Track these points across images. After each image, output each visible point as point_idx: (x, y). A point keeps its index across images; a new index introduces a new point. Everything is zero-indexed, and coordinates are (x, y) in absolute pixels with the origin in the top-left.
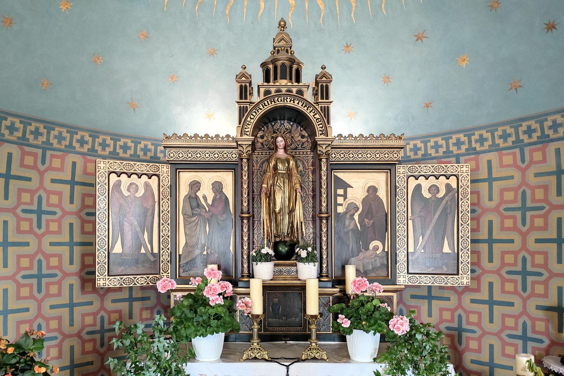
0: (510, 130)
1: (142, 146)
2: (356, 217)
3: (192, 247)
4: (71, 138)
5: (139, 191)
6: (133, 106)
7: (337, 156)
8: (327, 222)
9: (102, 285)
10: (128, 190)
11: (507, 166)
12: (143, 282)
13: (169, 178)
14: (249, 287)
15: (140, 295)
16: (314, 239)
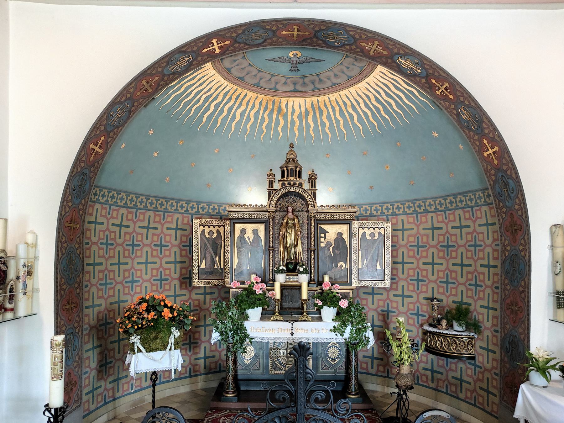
0: (411, 205)
1: (212, 207)
2: (331, 249)
4: (177, 205)
6: (208, 186)
7: (320, 217)
8: (314, 253)
10: (209, 235)
11: (411, 223)
14: (274, 286)
15: (209, 291)
16: (308, 260)
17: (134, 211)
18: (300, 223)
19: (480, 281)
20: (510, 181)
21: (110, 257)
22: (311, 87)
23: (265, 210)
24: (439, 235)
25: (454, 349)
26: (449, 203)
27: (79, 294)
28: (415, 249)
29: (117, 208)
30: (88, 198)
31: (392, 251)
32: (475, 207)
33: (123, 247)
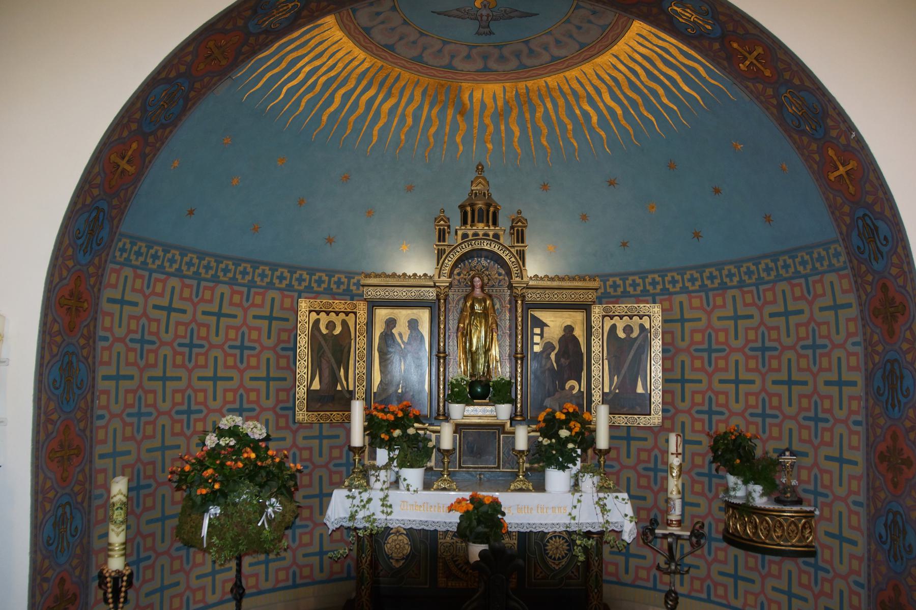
3: (386, 385)
4: (272, 275)
5: (337, 329)
7: (531, 296)
9: (301, 420)
10: (327, 328)
12: (339, 419)
13: (366, 315)
17: (195, 283)
18: (496, 307)
19: (824, 411)
20: (880, 224)
21: (148, 366)
22: (514, 63)
23: (432, 284)
24: (747, 329)
25: (778, 537)
26: (764, 270)
27: (84, 430)
28: (705, 355)
29: (163, 277)
30: (108, 255)
31: (664, 359)
32: (811, 275)
33: (173, 349)
